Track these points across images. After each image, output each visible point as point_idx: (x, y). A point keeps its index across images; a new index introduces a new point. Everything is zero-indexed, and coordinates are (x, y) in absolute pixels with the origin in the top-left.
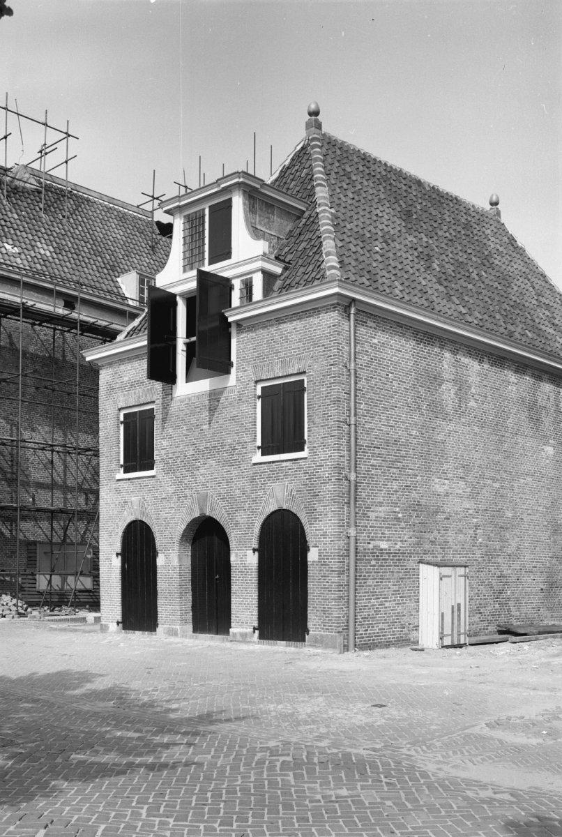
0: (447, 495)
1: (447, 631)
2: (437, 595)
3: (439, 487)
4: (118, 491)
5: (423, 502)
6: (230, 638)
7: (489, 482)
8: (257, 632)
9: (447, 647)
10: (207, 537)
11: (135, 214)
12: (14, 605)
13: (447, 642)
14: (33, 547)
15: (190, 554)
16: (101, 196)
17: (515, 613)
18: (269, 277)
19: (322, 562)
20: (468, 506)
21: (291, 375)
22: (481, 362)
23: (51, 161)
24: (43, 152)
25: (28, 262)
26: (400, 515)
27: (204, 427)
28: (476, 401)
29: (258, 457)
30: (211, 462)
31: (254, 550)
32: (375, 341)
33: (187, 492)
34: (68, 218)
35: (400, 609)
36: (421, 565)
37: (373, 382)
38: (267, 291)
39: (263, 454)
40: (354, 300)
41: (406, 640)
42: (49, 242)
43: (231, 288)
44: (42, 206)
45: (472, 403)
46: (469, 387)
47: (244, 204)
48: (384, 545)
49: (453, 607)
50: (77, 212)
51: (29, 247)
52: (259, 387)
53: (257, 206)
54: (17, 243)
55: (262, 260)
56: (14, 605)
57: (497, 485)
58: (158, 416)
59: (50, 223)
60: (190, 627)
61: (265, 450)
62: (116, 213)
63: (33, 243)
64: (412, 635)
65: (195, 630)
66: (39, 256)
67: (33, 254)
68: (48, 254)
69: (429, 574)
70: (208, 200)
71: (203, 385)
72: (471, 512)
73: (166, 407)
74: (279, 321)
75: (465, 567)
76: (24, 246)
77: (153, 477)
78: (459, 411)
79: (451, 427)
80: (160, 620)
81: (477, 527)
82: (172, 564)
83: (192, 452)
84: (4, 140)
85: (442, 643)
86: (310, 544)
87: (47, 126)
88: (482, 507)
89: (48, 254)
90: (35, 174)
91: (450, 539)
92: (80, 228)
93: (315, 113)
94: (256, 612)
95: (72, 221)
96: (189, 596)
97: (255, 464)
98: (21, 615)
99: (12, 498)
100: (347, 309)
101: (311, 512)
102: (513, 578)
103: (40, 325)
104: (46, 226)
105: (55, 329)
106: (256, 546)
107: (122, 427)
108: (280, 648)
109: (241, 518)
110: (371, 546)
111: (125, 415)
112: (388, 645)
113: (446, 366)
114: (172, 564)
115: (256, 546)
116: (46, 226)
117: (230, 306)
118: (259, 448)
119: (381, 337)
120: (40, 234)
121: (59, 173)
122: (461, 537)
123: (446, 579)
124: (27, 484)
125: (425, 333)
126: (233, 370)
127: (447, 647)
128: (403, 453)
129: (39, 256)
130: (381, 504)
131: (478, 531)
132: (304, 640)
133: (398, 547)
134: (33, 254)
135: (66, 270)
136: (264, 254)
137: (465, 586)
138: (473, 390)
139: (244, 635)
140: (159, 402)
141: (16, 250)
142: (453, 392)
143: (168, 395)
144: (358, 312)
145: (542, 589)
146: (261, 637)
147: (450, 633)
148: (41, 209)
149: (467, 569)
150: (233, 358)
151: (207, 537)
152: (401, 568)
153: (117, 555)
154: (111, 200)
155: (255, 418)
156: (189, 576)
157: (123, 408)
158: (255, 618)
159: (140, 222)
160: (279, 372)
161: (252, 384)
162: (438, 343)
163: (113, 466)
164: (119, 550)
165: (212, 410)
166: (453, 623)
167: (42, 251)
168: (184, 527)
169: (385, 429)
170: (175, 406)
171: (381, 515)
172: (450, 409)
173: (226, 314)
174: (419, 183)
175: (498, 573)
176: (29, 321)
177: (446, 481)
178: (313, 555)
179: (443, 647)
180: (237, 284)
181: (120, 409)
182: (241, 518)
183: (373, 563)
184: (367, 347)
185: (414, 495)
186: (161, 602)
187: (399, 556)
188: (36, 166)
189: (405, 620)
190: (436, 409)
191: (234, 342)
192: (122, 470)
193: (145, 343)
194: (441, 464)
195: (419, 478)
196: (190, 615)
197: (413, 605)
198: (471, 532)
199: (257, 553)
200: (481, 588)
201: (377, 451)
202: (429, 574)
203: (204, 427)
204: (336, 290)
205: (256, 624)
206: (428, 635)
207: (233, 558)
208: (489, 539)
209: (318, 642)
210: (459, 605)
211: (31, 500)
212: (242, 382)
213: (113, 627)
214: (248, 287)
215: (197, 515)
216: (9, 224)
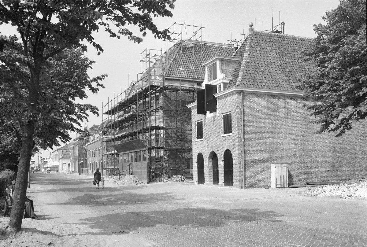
0: (282, 142)
1: (279, 182)
2: (277, 172)
3: (278, 140)
4: (196, 144)
5: (272, 145)
6: (218, 185)
7: (301, 137)
8: (224, 183)
9: (279, 188)
10: (213, 156)
11: (227, 47)
12: (181, 178)
13: (279, 186)
14: (189, 160)
15: (212, 162)
16: (215, 43)
17: (314, 177)
18: (225, 84)
19: (206, 165)
20: (292, 145)
21: (226, 113)
22: (296, 100)
23: (197, 36)
24: (195, 33)
25: (187, 72)
26: (262, 150)
27: (212, 126)
28: (295, 113)
29: (223, 135)
30: (214, 136)
31: (223, 161)
32: (252, 100)
33: (209, 145)
34: (202, 54)
35: (263, 177)
36: (271, 164)
37: (251, 112)
38: (225, 88)
39: (224, 134)
40: (242, 91)
41: (266, 186)
42: (194, 64)
43: (216, 88)
44: (193, 52)
45: (293, 114)
46: (292, 109)
47: (219, 63)
48: (256, 158)
49: (281, 176)
50: (206, 52)
51: (188, 67)
52: (223, 115)
53: (224, 63)
54: (184, 67)
55: (222, 80)
56: (181, 178)
57: (305, 138)
58: (203, 123)
59: (195, 57)
60: (213, 183)
61: (225, 133)
62: (220, 48)
63: (189, 66)
64: (268, 185)
65: (214, 183)
66: (190, 70)
67: (188, 69)
68: (194, 68)
69: (273, 166)
70: (176, 82)
71: (212, 114)
72: (293, 147)
73: (205, 121)
74: (226, 97)
75: (286, 164)
76: (186, 67)
77: (203, 140)
78: (287, 117)
79: (283, 122)
80: (205, 181)
81: (296, 152)
82: (208, 164)
83: (210, 134)
84: (178, 35)
85: (277, 186)
86: (233, 159)
87: (194, 26)
88: (298, 145)
89: (194, 68)
90: (192, 42)
91: (284, 156)
92: (206, 57)
93: (251, 26)
94: (223, 178)
95: (203, 55)
96: (212, 174)
97: (222, 137)
98: (182, 181)
99: (182, 145)
100: (240, 93)
101: (233, 150)
102: (314, 167)
103: (189, 92)
104: (194, 59)
105: (194, 93)
106: (223, 160)
107: (197, 126)
108: (228, 187)
109: (220, 152)
110: (251, 159)
111: (197, 123)
112: (258, 187)
113: (281, 104)
114: (208, 164)
115: (223, 160)
116: (194, 59)
117: (216, 93)
118: (223, 132)
119: (254, 99)
120: (192, 62)
121: (199, 40)
122: (289, 155)
123: (278, 168)
124: (187, 141)
125: (271, 95)
126: (217, 110)
127: (279, 188)
128: (263, 131)
129: (190, 70)
130: (255, 147)
131: (296, 153)
132: (232, 186)
133: (262, 159)
134: (188, 69)
135: (199, 73)
136: (224, 78)
137: (286, 170)
138: (293, 110)
139: (221, 184)
140: (203, 119)
141: (183, 69)
142: (284, 112)
143: (205, 117)
144: (243, 94)
145: (328, 170)
146: (225, 185)
147: (280, 184)
148: (193, 53)
149: (287, 165)
150: (217, 107)
151: (213, 156)
152: (264, 166)
153: (196, 162)
154: (219, 44)
155: (222, 124)
156: (212, 168)
157: (223, 113)
158: (223, 180)
159: (228, 49)
160: (226, 111)
161: (221, 115)
162: (277, 97)
163: (195, 138)
164: (197, 161)
165: (214, 121)
166: (281, 181)
167: (192, 68)
168: (209, 154)
169: (256, 125)
170: (207, 120)
171: (254, 150)
172: (283, 116)
173: (214, 95)
174: (294, 38)
175: (306, 166)
176: (184, 92)
177: (282, 138)
178: (234, 162)
179: (277, 188)
180: (218, 86)
181: (196, 121)
182: (220, 152)
183: (252, 163)
184: (248, 103)
185: (268, 143)
186: (205, 175)
187: (263, 162)
188: (192, 39)
189: (265, 180)
190: (277, 117)
191: (217, 102)
192: (223, 133)
193: (196, 104)
194: (279, 133)
195: (270, 138)
196: (212, 179)
197: (269, 175)
198: (293, 153)
199: (223, 162)
200: (298, 170)
201: (253, 132)
202: (273, 166)
203: (212, 126)
204: (235, 89)
205: (224, 181)
206: (273, 185)
207: (219, 163)
208: (302, 155)
209: (235, 186)
210: (284, 176)
211: (188, 146)
212: (219, 114)
213: (196, 183)
214: (220, 86)
215: (211, 151)
216: (182, 61)
